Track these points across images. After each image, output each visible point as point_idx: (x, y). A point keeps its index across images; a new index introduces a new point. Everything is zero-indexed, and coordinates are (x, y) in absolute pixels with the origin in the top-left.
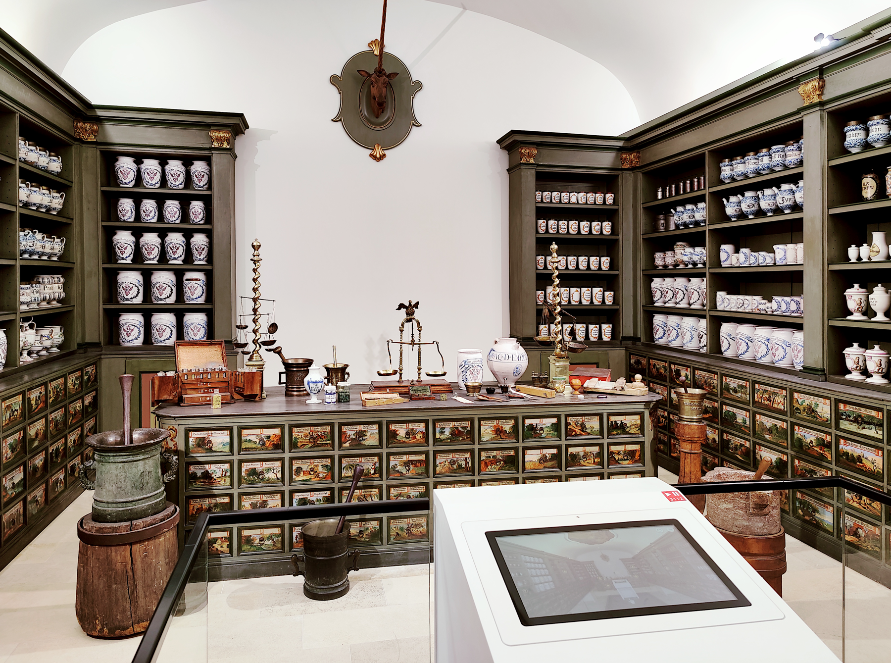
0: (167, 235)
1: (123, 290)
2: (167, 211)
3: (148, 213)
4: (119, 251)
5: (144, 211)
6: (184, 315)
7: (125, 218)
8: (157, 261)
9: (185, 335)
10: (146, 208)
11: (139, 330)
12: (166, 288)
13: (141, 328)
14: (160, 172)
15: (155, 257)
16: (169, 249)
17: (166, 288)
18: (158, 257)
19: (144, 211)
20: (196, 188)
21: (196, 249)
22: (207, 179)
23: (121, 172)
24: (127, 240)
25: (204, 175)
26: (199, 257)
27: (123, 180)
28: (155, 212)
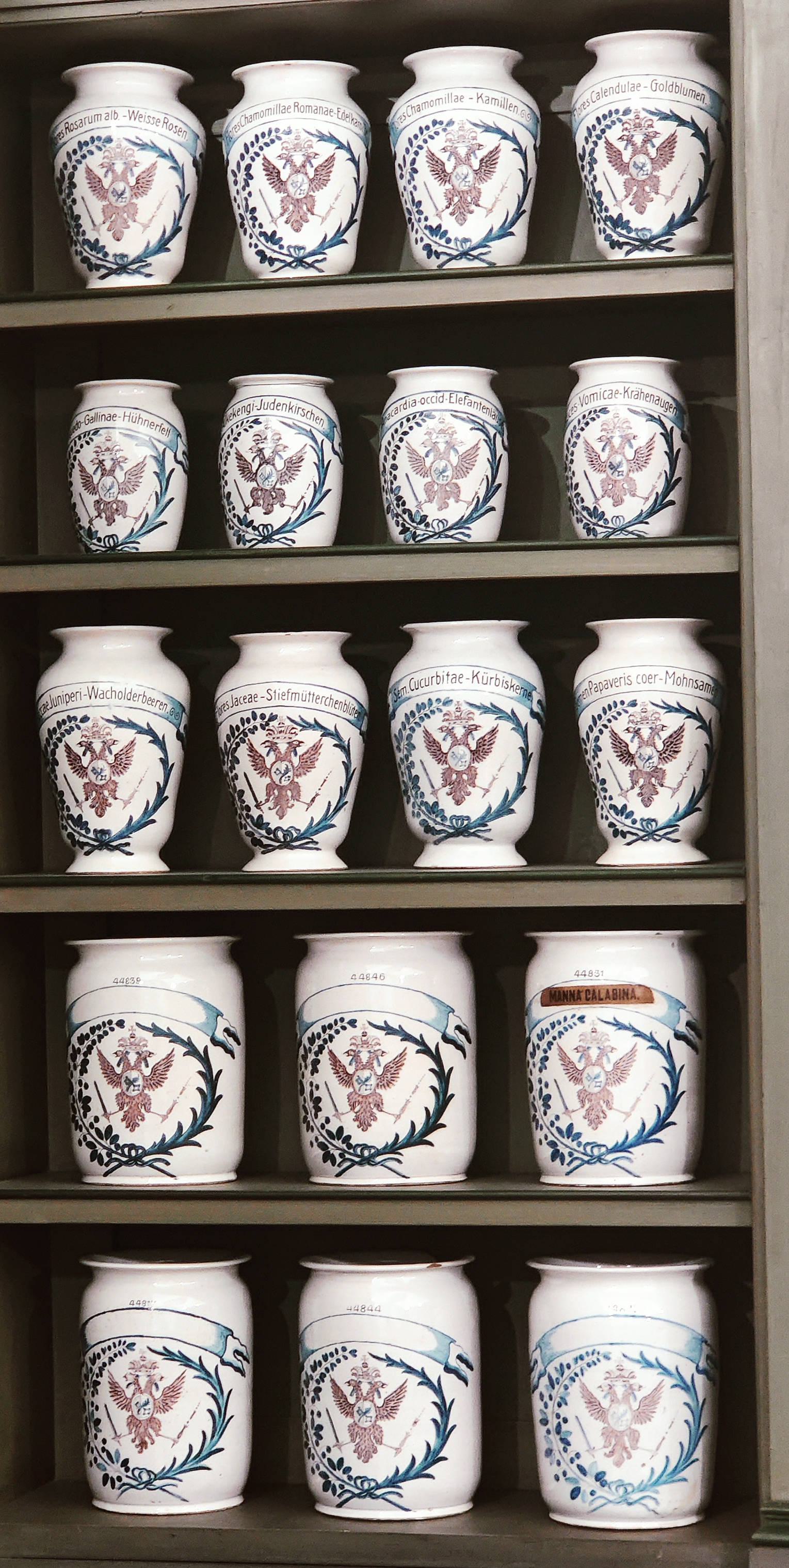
0: (592, 643)
1: (103, 1082)
2: (403, 455)
3: (270, 475)
4: (78, 783)
5: (244, 467)
6: (536, 1278)
7: (121, 528)
8: (341, 851)
9: (542, 1445)
10: (259, 439)
11: (220, 1397)
12: (398, 1062)
13: (228, 1377)
14: (359, 149)
15: (325, 824)
16: (608, 754)
17: (398, 1062)
18: (342, 821)
19: (244, 467)
20: (618, 255)
21: (618, 743)
22: (697, 170)
23: (95, 184)
24: (132, 696)
25: (671, 141)
26: (641, 812)
27: (106, 239)
28: (322, 468)
